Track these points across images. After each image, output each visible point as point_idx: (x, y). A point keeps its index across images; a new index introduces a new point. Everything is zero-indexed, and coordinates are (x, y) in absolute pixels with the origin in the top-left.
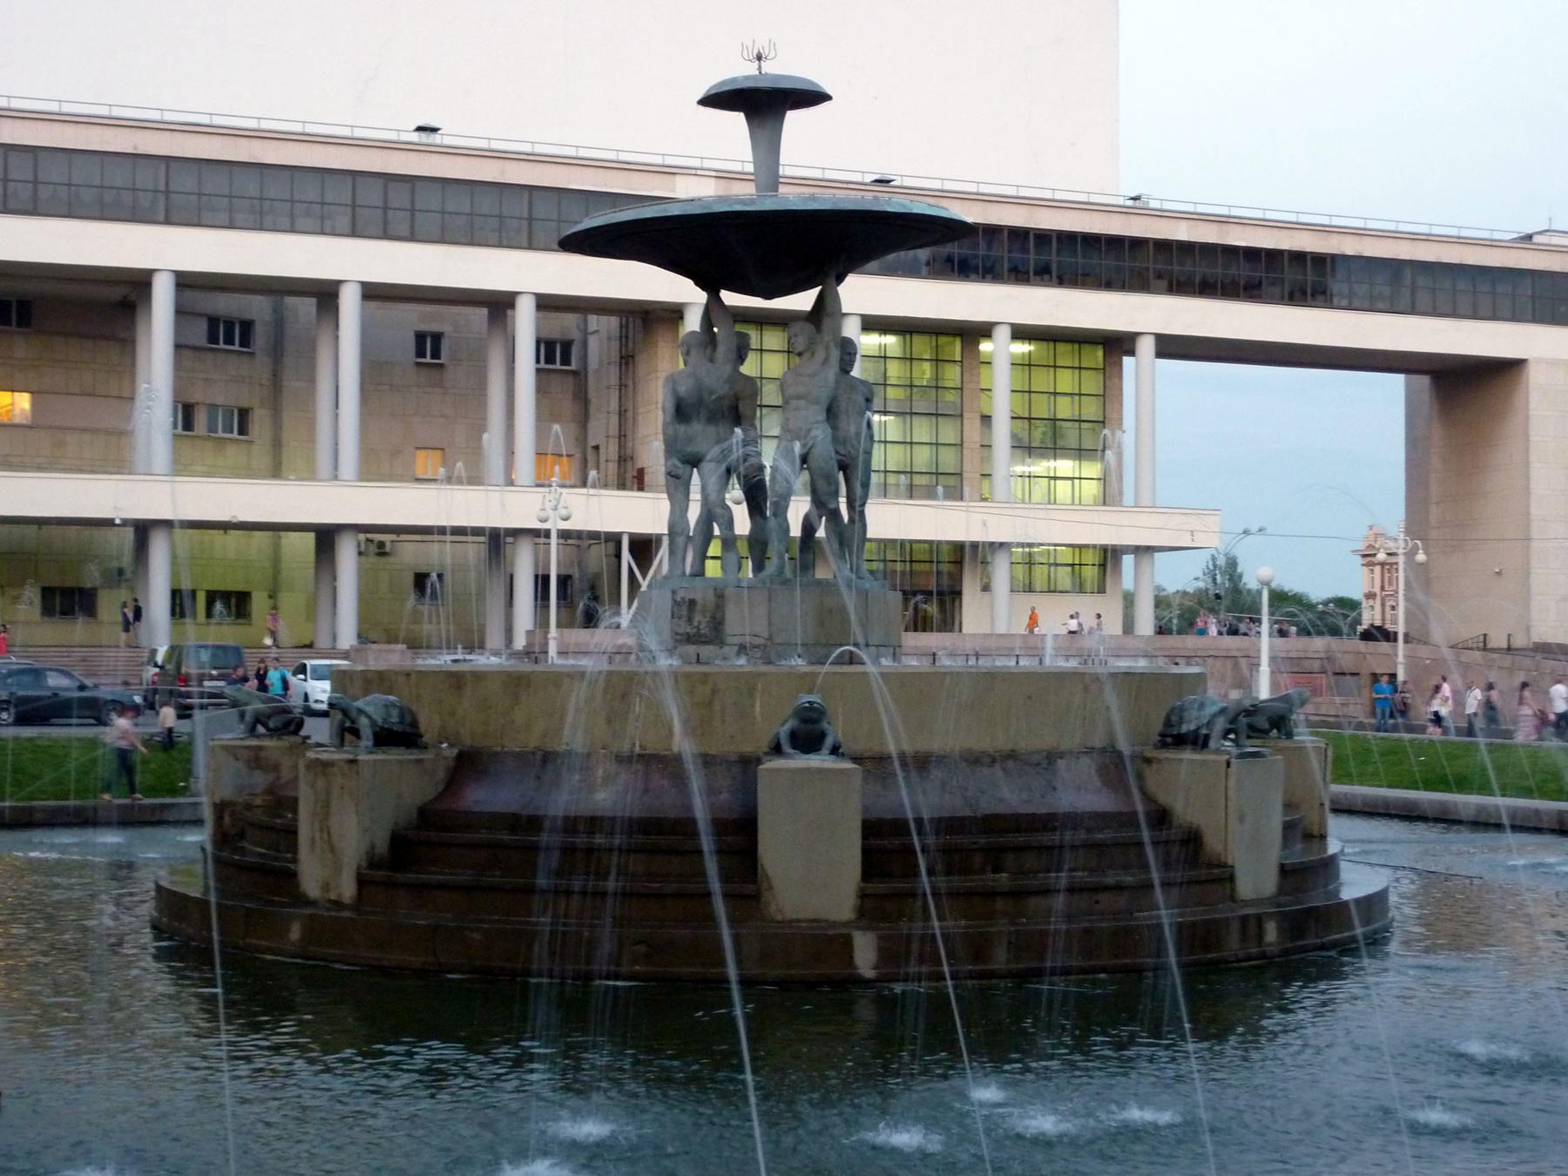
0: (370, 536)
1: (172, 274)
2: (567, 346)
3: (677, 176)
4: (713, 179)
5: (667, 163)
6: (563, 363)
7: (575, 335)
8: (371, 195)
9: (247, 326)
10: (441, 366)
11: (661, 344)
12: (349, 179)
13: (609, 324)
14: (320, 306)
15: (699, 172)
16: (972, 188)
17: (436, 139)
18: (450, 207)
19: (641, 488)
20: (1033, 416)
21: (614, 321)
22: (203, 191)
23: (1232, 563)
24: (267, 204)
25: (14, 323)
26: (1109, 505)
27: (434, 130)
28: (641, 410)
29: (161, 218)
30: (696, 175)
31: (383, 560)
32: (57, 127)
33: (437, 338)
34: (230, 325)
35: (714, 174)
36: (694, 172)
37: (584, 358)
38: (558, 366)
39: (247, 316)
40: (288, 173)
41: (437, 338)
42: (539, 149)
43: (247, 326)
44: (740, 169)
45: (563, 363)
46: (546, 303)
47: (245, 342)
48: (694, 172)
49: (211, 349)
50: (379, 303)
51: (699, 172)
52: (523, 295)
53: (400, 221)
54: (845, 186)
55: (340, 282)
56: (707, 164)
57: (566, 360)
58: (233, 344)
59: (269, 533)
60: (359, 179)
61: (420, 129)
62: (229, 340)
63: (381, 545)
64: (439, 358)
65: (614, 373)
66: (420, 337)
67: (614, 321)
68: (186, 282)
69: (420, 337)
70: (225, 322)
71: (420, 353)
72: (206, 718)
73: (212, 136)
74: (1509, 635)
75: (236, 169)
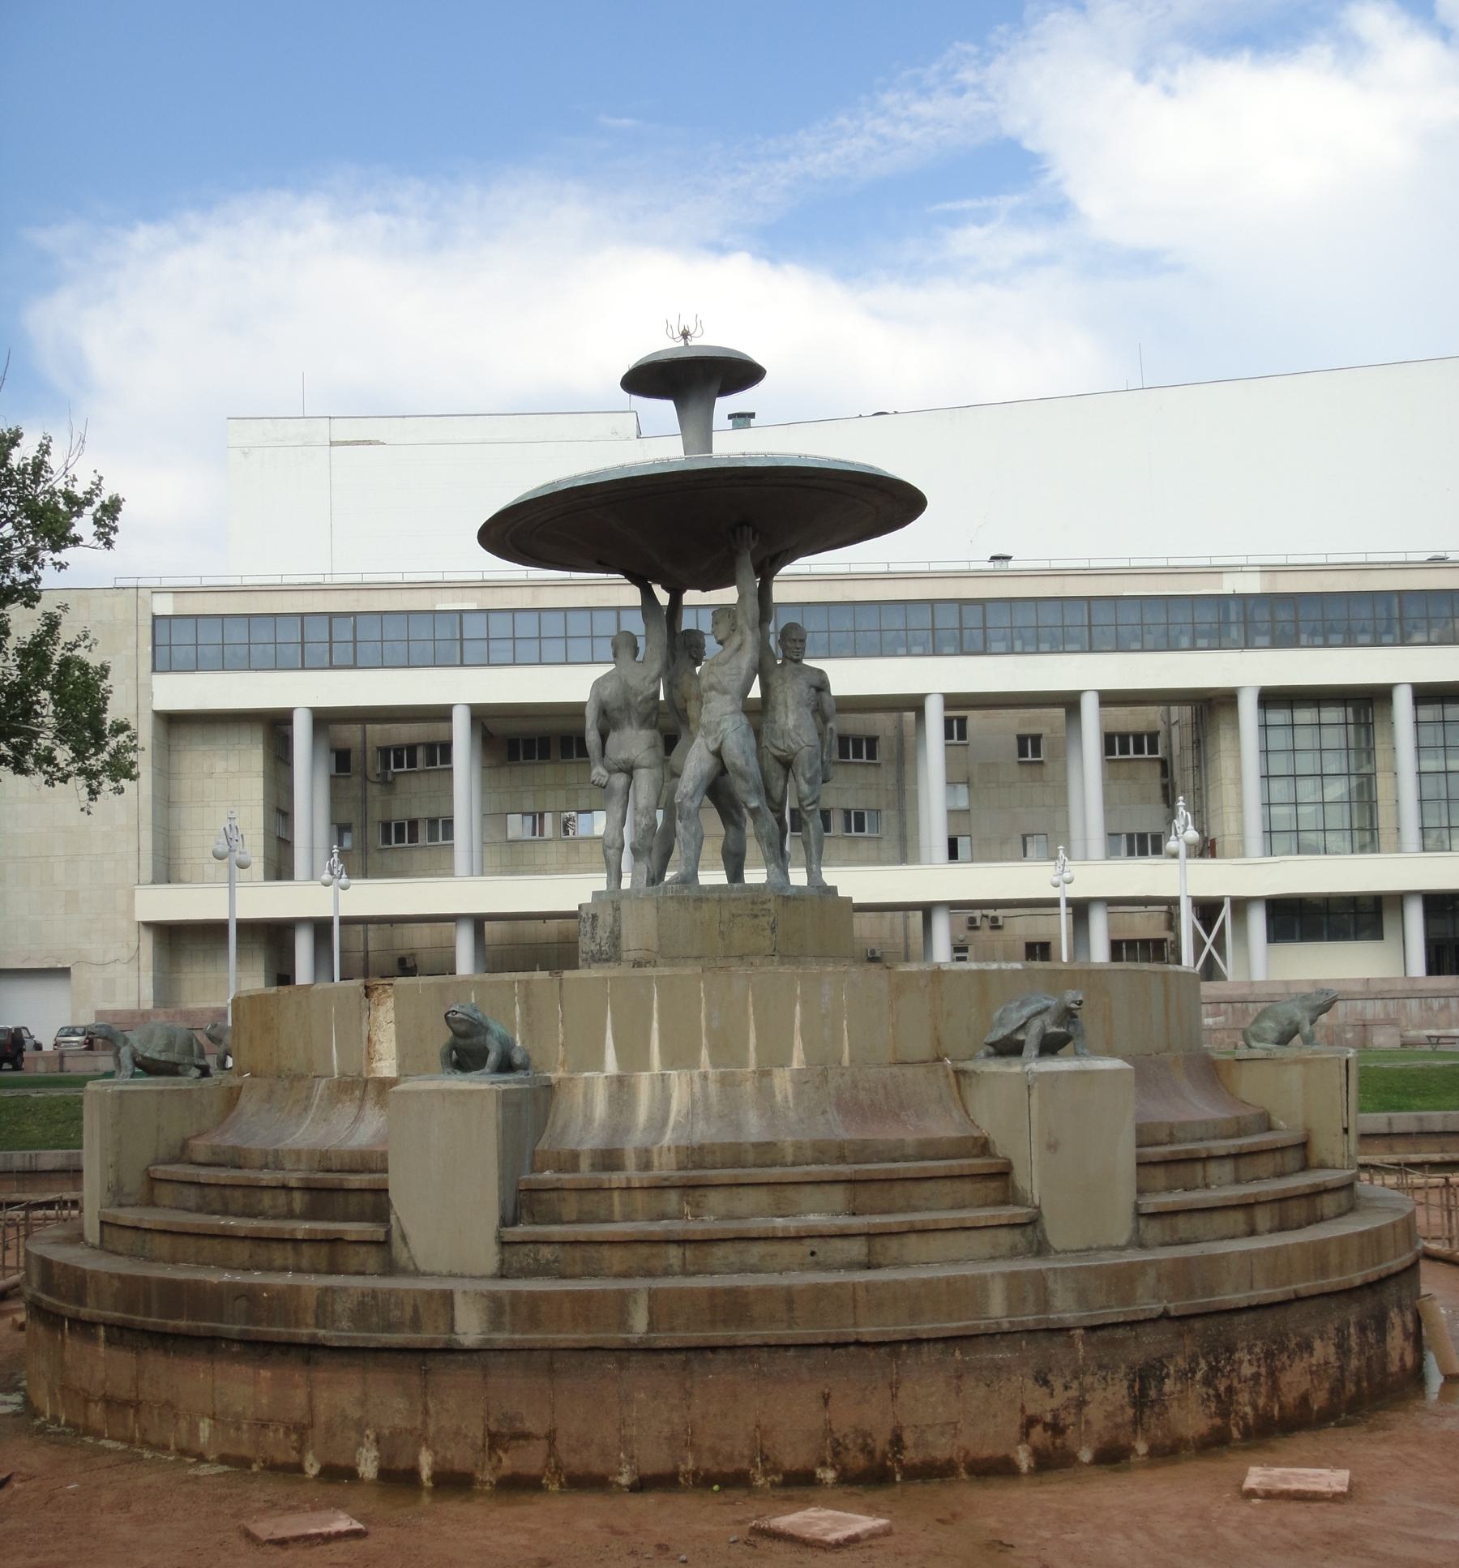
0: (985, 912)
1: (308, 710)
2: (1153, 737)
3: (1224, 575)
4: (1258, 574)
5: (1213, 563)
6: (1150, 753)
7: (1160, 726)
8: (318, 632)
9: (872, 741)
10: (1041, 763)
11: (1221, 727)
12: (613, 614)
13: (1182, 714)
14: (1068, 713)
15: (1244, 569)
16: (1322, 560)
17: (1011, 565)
18: (1019, 622)
19: (1214, 856)
20: (1324, 773)
21: (1187, 711)
22: (1145, 622)
23: (783, 905)
24: (1145, 627)
25: (575, 755)
26: (1330, 854)
27: (1008, 558)
28: (1210, 787)
29: (931, 652)
30: (1241, 571)
31: (996, 932)
32: (396, 595)
33: (1036, 739)
34: (857, 742)
35: (1258, 569)
36: (1239, 569)
37: (1169, 747)
38: (1146, 755)
39: (872, 733)
40: (1032, 604)
41: (1036, 739)
42: (1372, 558)
43: (872, 741)
44: (1208, 564)
45: (1150, 753)
46: (1108, 699)
47: (872, 754)
48: (1239, 569)
49: (843, 763)
50: (984, 712)
51: (1244, 569)
52: (931, 696)
53: (342, 652)
54: (1387, 566)
55: (294, 709)
56: (1252, 561)
57: (1153, 749)
58: (862, 758)
59: (901, 913)
60: (570, 615)
61: (994, 558)
62: (1124, 750)
63: (995, 919)
64: (1040, 756)
65: (1189, 755)
66: (1022, 740)
67: (1187, 711)
68: (324, 720)
69: (1022, 740)
70: (853, 740)
71: (1023, 752)
72: (721, 1073)
73: (523, 589)
74: (65, 972)
75: (857, 608)
